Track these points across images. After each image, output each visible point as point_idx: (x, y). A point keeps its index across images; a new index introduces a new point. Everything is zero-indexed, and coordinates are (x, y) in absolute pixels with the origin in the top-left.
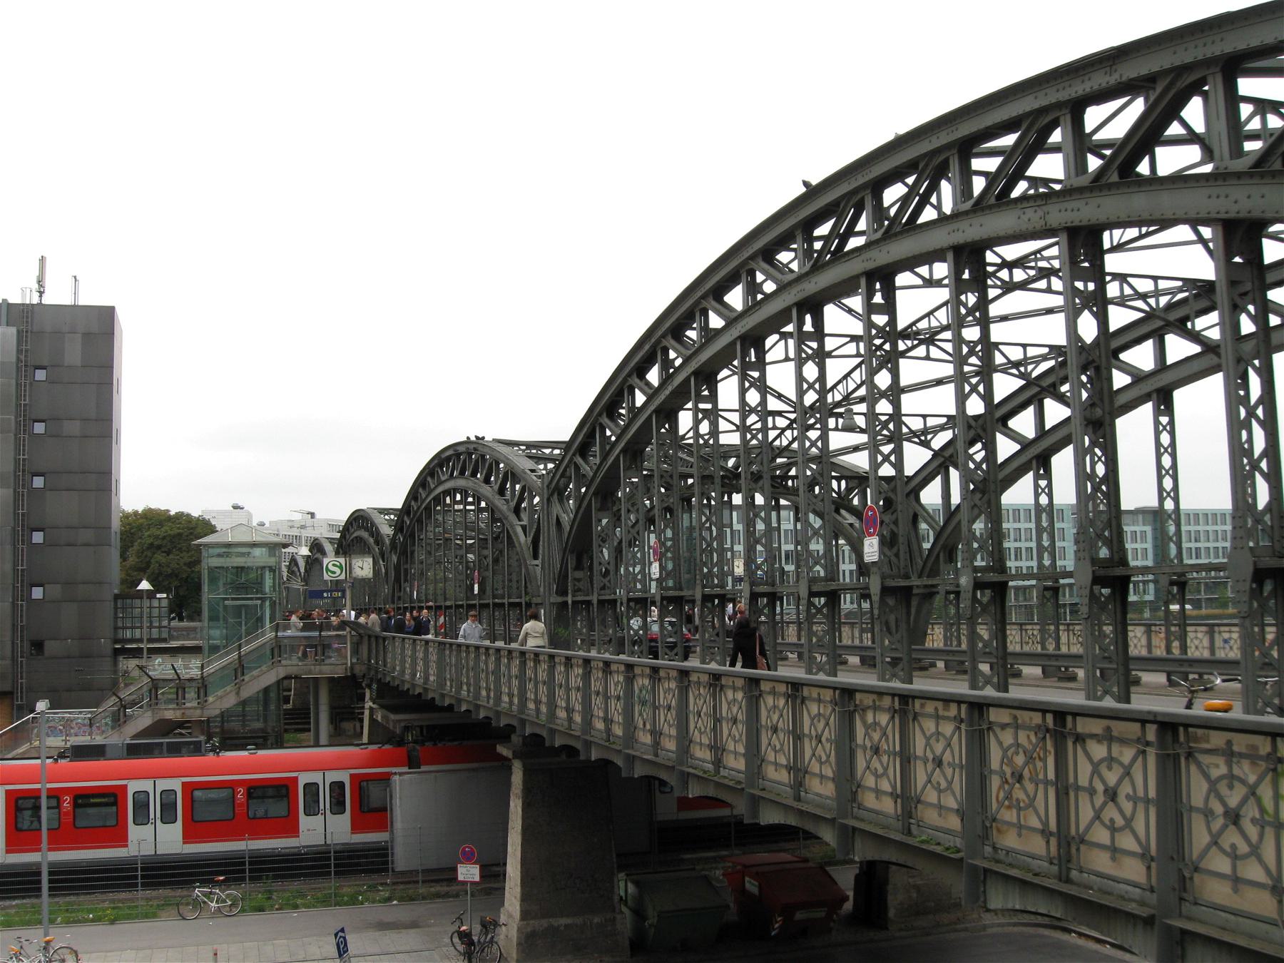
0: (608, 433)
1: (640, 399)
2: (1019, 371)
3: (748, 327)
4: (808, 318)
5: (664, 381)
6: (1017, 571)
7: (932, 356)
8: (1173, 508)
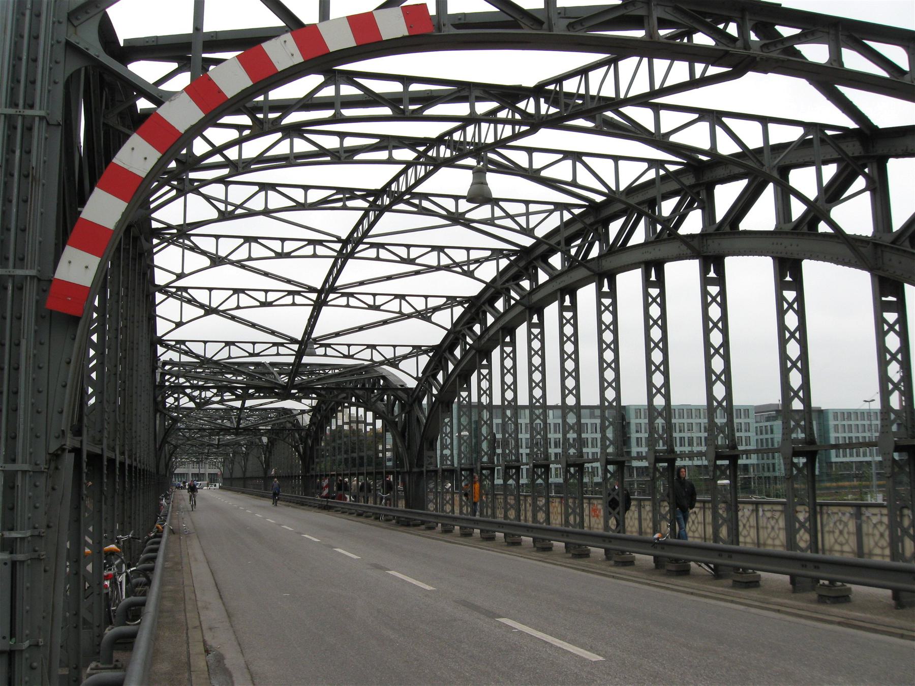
2: (463, 269)
4: (567, 298)
6: (869, 439)
8: (664, 404)
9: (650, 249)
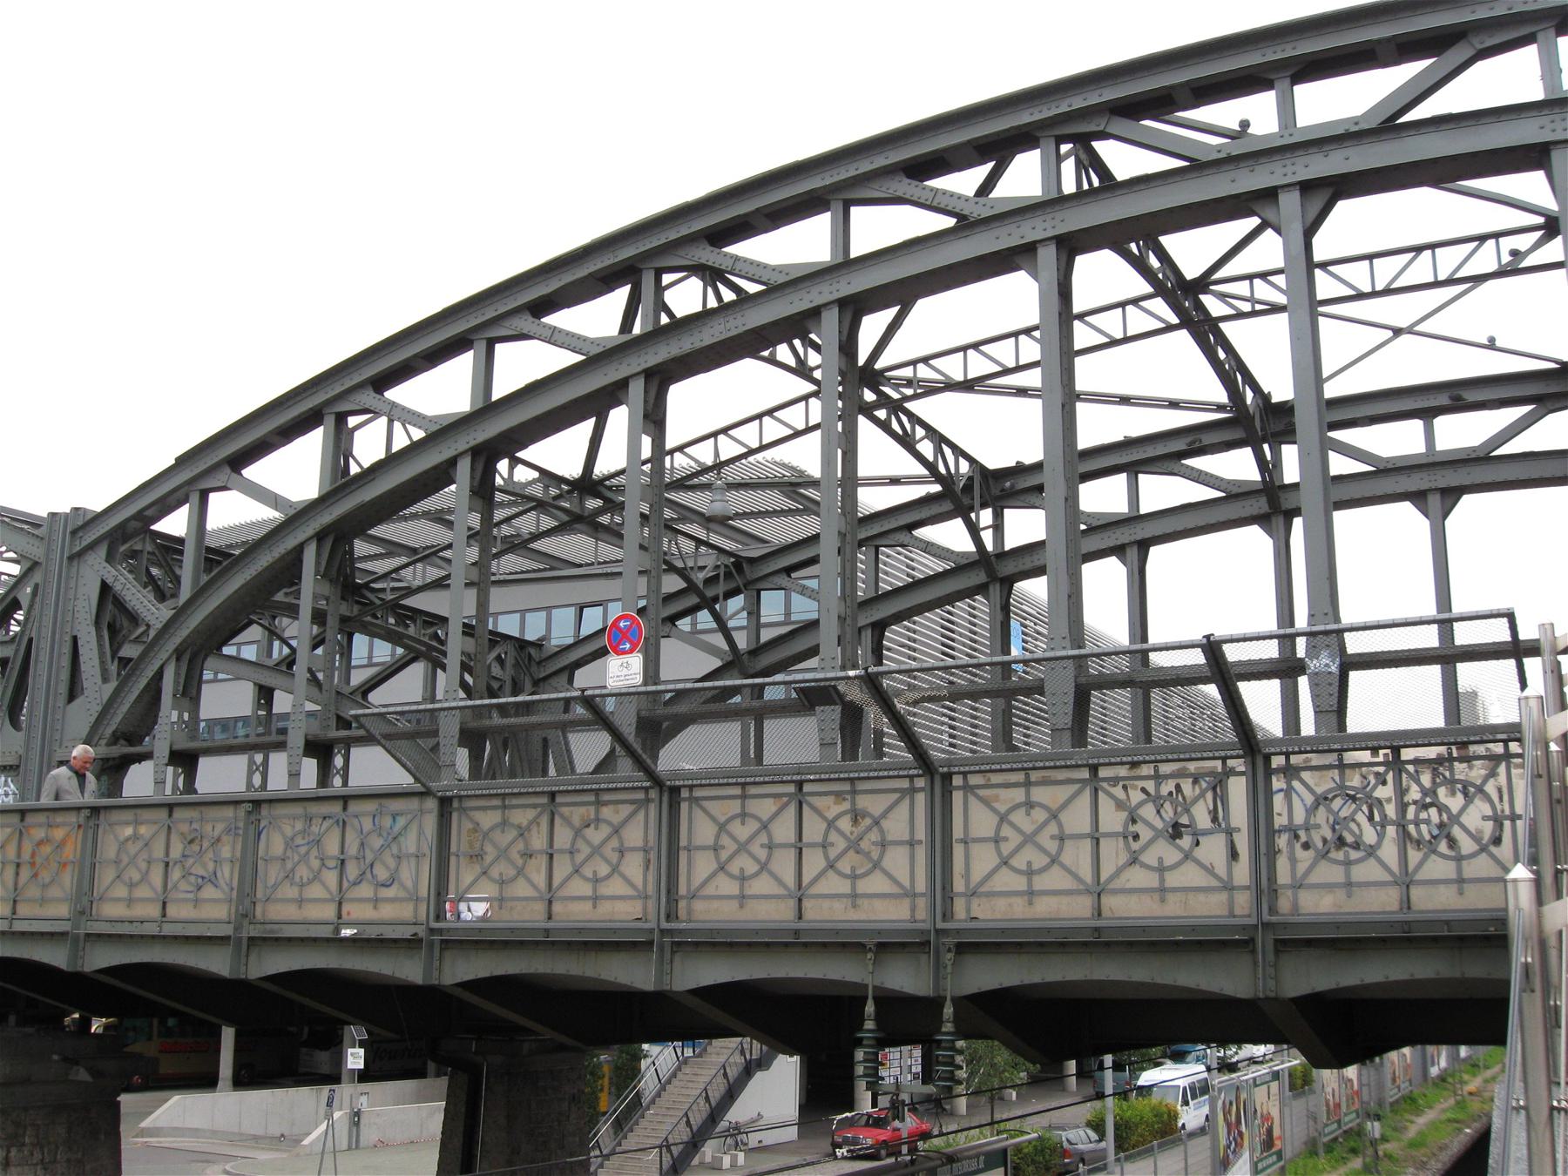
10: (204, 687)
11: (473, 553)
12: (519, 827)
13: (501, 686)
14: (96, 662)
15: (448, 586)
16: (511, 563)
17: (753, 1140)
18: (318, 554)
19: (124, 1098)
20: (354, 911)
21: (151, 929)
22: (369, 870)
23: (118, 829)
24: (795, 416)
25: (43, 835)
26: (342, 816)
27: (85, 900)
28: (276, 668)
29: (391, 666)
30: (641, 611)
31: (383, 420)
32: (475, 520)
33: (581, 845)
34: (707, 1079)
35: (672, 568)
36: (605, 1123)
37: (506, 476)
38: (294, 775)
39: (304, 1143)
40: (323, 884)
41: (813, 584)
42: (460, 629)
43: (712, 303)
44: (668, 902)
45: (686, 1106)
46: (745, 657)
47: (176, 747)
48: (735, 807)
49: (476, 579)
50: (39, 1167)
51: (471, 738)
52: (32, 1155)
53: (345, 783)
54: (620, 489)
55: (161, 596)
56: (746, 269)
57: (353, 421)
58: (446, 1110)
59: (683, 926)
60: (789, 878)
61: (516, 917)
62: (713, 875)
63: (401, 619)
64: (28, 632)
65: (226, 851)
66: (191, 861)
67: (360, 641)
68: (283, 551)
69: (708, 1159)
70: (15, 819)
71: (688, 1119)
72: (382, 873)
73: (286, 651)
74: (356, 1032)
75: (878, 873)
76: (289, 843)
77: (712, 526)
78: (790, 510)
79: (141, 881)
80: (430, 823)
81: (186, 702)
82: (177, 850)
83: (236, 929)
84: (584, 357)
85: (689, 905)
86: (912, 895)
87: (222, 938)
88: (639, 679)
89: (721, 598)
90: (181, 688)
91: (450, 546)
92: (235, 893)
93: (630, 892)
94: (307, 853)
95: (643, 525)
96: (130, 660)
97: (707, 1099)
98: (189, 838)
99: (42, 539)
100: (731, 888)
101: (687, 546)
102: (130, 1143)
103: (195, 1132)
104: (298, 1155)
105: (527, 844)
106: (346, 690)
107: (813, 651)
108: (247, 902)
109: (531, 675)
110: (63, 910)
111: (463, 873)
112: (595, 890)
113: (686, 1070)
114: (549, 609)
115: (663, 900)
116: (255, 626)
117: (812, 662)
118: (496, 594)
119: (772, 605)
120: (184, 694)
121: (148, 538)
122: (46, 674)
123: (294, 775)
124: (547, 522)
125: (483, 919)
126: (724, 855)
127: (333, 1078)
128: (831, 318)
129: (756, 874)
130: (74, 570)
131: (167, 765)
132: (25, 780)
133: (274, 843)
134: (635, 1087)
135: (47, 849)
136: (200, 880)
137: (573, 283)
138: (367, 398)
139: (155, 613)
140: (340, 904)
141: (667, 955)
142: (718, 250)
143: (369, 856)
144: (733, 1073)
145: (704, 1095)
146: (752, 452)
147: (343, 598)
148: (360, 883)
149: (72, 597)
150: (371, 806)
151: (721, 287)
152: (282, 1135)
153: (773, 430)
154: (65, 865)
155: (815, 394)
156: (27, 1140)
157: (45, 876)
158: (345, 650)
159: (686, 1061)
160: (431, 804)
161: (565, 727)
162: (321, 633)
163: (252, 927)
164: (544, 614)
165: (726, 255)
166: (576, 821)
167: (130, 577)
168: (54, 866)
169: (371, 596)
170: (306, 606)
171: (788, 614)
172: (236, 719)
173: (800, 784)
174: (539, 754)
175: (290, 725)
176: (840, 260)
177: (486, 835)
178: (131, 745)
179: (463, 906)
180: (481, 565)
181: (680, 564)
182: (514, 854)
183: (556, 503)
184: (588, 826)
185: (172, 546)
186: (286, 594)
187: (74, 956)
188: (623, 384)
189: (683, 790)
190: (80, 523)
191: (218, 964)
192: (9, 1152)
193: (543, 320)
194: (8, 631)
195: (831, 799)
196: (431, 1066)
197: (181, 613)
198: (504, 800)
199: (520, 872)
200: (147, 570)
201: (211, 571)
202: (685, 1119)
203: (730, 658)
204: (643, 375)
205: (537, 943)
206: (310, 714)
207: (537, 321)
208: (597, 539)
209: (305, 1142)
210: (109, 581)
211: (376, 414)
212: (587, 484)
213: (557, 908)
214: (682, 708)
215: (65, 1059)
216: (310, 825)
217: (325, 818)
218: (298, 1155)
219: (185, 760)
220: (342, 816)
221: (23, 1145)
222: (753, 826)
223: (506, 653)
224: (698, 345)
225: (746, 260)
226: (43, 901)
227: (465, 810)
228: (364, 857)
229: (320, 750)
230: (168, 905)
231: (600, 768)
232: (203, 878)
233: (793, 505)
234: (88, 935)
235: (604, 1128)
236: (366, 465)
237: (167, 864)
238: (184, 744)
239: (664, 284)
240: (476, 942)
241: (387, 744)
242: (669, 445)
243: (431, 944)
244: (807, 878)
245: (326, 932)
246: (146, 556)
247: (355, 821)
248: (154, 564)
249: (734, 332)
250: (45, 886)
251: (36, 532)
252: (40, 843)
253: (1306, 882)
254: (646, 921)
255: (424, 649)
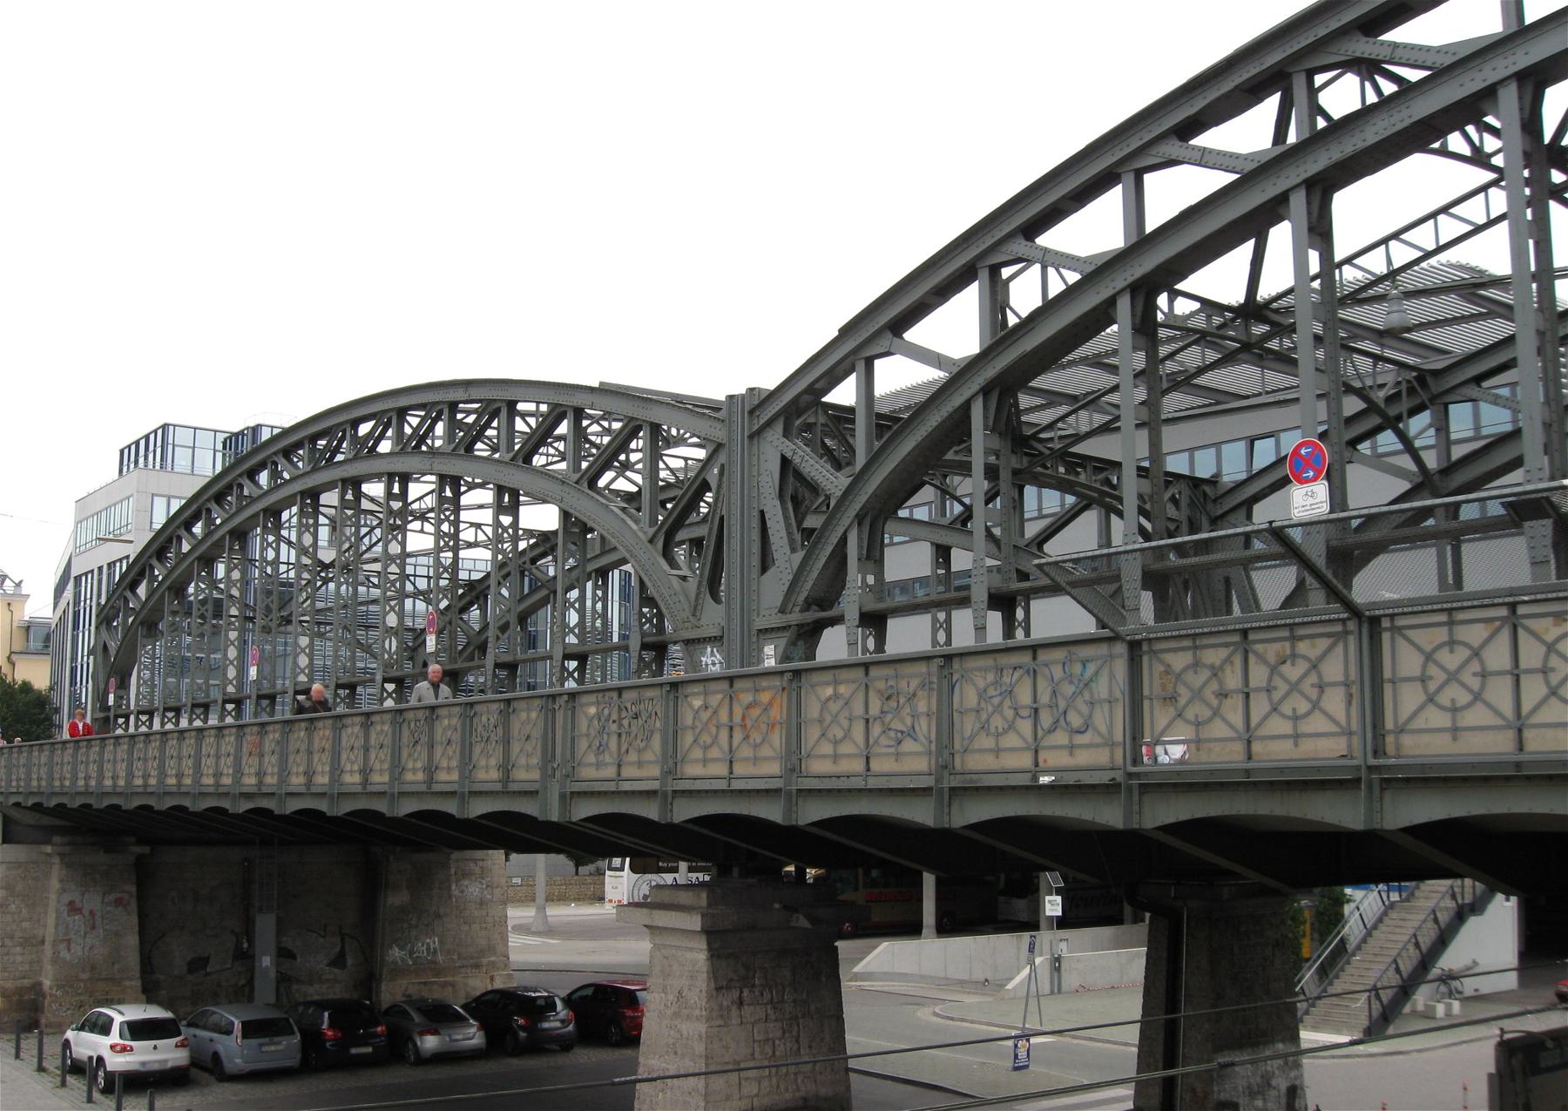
0: (157, 573)
1: (186, 547)
3: (268, 503)
5: (207, 535)
7: (425, 530)
9: (395, 459)
10: (886, 550)
11: (1141, 394)
12: (1212, 667)
13: (1178, 527)
14: (783, 533)
15: (1118, 429)
16: (1174, 402)
17: (1469, 986)
18: (986, 408)
19: (840, 944)
20: (1050, 758)
21: (858, 783)
22: (1062, 719)
23: (819, 690)
24: (1474, 210)
25: (751, 699)
26: (1032, 665)
27: (794, 758)
28: (950, 527)
29: (1062, 517)
30: (1323, 436)
31: (1037, 267)
32: (1139, 360)
33: (1278, 682)
34: (1416, 924)
35: (1349, 389)
36: (1309, 969)
37: (1166, 310)
38: (981, 629)
39: (1007, 987)
40: (1018, 733)
41: (1505, 392)
42: (1134, 472)
43: (1372, 98)
44: (1374, 737)
45: (1394, 953)
46: (1436, 478)
47: (865, 609)
48: (1442, 634)
49: (1146, 419)
50: (769, 1007)
51: (1155, 580)
52: (762, 995)
53: (1027, 634)
54: (1288, 311)
55: (838, 465)
56: (1406, 55)
57: (1006, 272)
58: (1147, 954)
59: (1392, 761)
60: (1507, 707)
61: (1214, 758)
62: (1421, 708)
63: (1071, 469)
64: (719, 511)
65: (922, 706)
66: (889, 717)
67: (1030, 492)
68: (951, 410)
69: (1420, 1007)
70: (725, 685)
71: (1397, 965)
72: (1075, 720)
73: (958, 509)
74: (1051, 878)
75: (1479, 705)
76: (982, 694)
77: (1386, 341)
78: (1473, 315)
79: (845, 738)
80: (1121, 668)
81: (870, 565)
82: (875, 707)
83: (937, 781)
84: (1238, 176)
85: (1397, 739)
86: (1113, 745)
87: (924, 789)
88: (1326, 508)
89: (1405, 415)
90: (865, 552)
91: (1115, 388)
92: (933, 747)
93: (1333, 728)
94: (1001, 703)
95: (1316, 348)
96: (813, 530)
97: (1417, 945)
98: (886, 695)
99: (723, 421)
100: (1442, 720)
101: (1364, 364)
102: (847, 985)
103: (903, 977)
104: (1003, 999)
105: (1221, 683)
106: (1021, 543)
107: (1517, 463)
108: (946, 753)
109: (1208, 514)
110: (775, 768)
111: (1157, 717)
112: (1295, 727)
113: (1393, 915)
114: (1218, 445)
115: (1369, 735)
116: (927, 487)
117: (1516, 476)
118: (1167, 431)
119: (1460, 418)
120: (868, 558)
121: (820, 411)
122: (739, 549)
123: (981, 629)
124: (1212, 356)
125: (1181, 761)
126: (1432, 687)
127: (1032, 925)
128: (1509, 97)
129: (1469, 705)
130: (755, 448)
131: (858, 627)
132: (729, 650)
133: (967, 696)
134: (1339, 933)
135: (755, 713)
136: (899, 735)
137: (1218, 100)
138: (1019, 247)
139: (833, 482)
140: (1036, 752)
141: (1136, 798)
142: (1374, 40)
143: (1062, 704)
144: (1444, 918)
145: (1413, 940)
146: (1428, 255)
147: (1013, 452)
148: (1055, 729)
149: (755, 474)
150: (1059, 654)
151: (1380, 81)
152: (987, 980)
153: (1449, 228)
154: (773, 726)
155: (1494, 183)
156: (757, 982)
157: (756, 737)
158: (1018, 505)
159: (1392, 905)
160: (1121, 649)
161: (1247, 564)
162: (993, 488)
163: (952, 777)
164: (1213, 450)
165: (1383, 43)
166: (1272, 658)
167: (808, 449)
168: (764, 727)
169: (1040, 447)
170: (978, 461)
171: (1477, 428)
172: (914, 580)
173: (1513, 607)
174: (1222, 595)
175: (972, 581)
176: (1514, 28)
177: (1178, 676)
178: (823, 610)
179: (1159, 750)
180: (1151, 404)
181: (1357, 384)
182: (1208, 694)
183: (1220, 332)
184: (1284, 662)
185: (843, 415)
186: (956, 452)
187: (788, 811)
188: (1282, 199)
189: (1383, 619)
190: (755, 402)
191: (921, 814)
192: (741, 992)
193: (1192, 142)
194: (699, 513)
195: (1550, 620)
196: (1128, 910)
197: (858, 479)
198: (1194, 640)
199: (1216, 712)
200: (823, 442)
201: (882, 437)
202: (1394, 966)
203: (1420, 479)
204: (1304, 186)
205: (1238, 784)
206: (990, 569)
207: (1185, 144)
208: (1263, 368)
209: (1009, 987)
210: (789, 455)
211: (1029, 262)
212: (1252, 309)
213: (1257, 747)
214: (1374, 534)
215: (786, 907)
216: (1002, 676)
217: (1015, 668)
218: (1003, 999)
219: (875, 621)
220: (1032, 665)
221: (754, 986)
222: (1462, 654)
223: (1180, 493)
224: (1361, 145)
225: (1405, 46)
226: (756, 760)
227: (1155, 652)
228: (1057, 705)
229: (1003, 602)
230: (734, 764)
231: (1288, 602)
232: (902, 732)
233: (1475, 309)
234: (799, 791)
235: (1308, 975)
236: (1024, 315)
237: (867, 721)
238: (872, 606)
239: (1316, 86)
240: (1175, 785)
241: (1073, 591)
242: (1338, 257)
243: (1130, 788)
244: (1526, 707)
245: (1024, 780)
246: (819, 428)
247: (1046, 671)
248: (826, 435)
249: (1399, 127)
250: (756, 746)
251: (717, 415)
252: (749, 707)
253: (1408, 727)
254: (1352, 758)
255: (1096, 495)
